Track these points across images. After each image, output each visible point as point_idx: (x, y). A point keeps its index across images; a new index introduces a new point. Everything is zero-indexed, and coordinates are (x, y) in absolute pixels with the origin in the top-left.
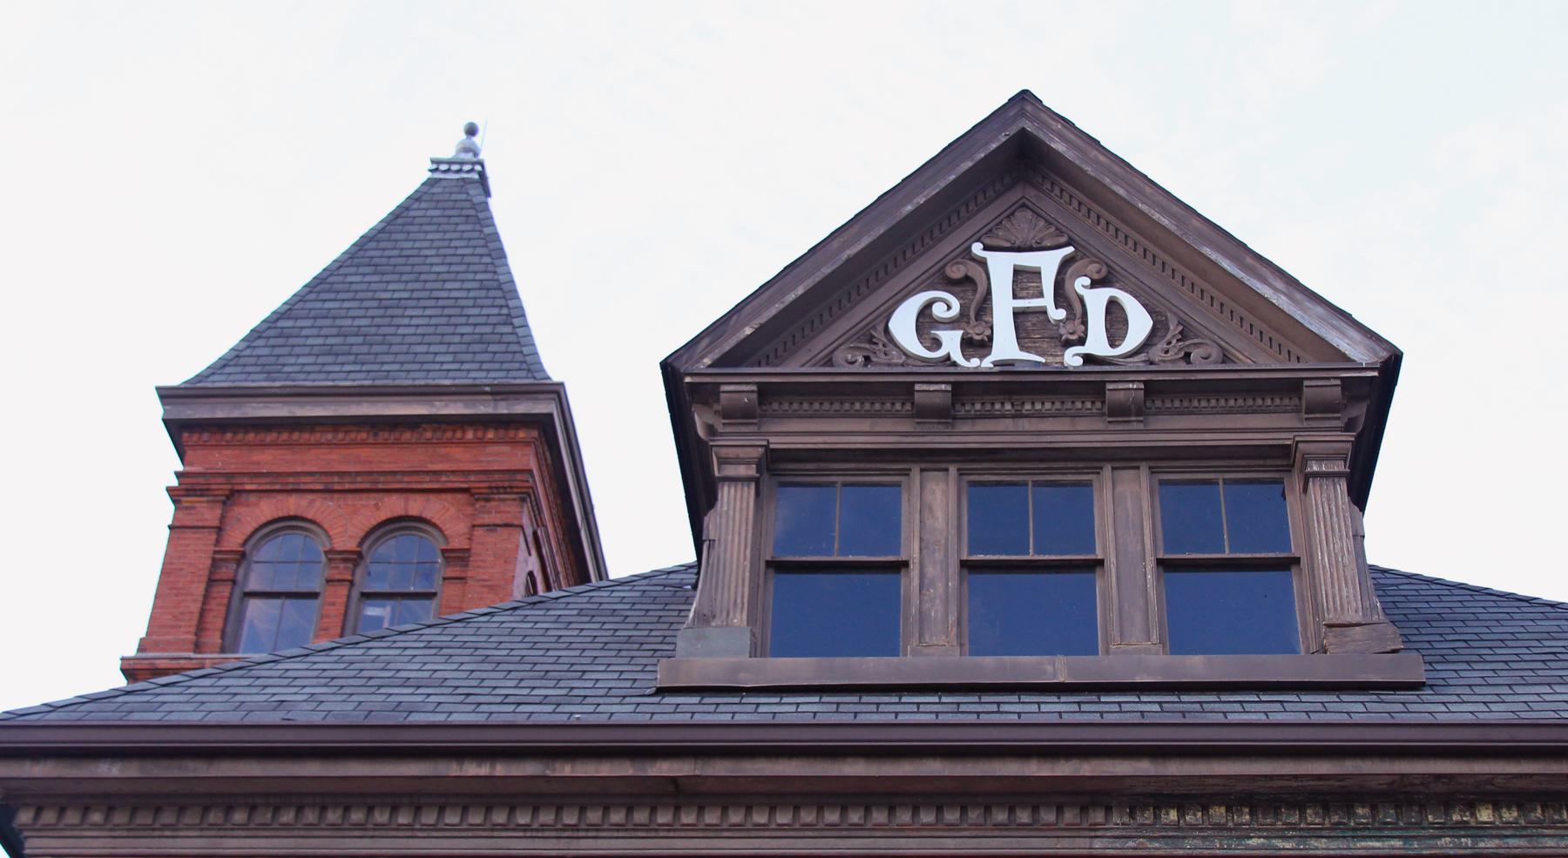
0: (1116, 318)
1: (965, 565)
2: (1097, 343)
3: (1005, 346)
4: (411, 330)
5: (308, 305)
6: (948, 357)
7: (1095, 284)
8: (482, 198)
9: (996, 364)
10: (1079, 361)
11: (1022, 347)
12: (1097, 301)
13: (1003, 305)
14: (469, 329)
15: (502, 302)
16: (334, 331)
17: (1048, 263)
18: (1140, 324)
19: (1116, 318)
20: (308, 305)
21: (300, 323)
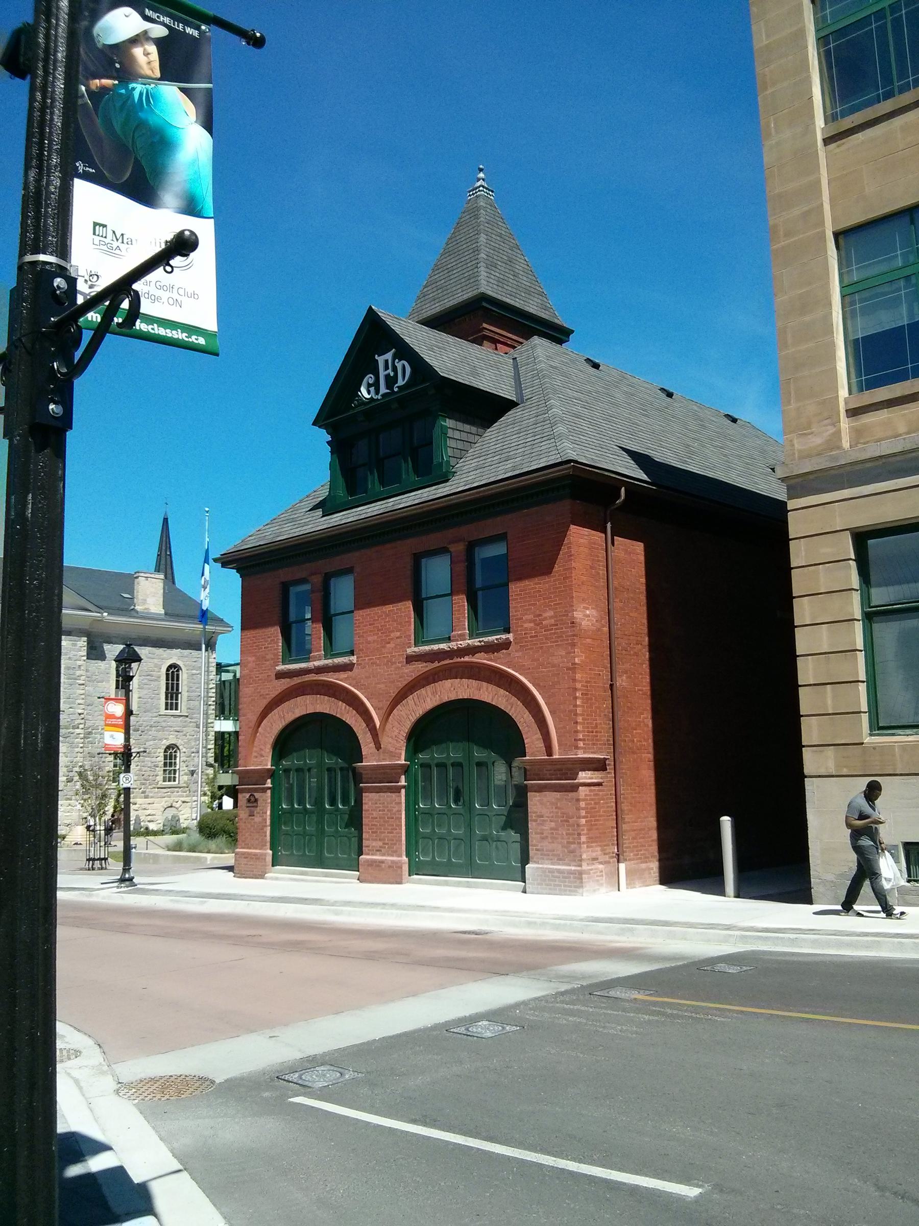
2: (401, 382)
3: (383, 390)
12: (399, 365)
13: (382, 374)
17: (389, 356)
18: (408, 370)
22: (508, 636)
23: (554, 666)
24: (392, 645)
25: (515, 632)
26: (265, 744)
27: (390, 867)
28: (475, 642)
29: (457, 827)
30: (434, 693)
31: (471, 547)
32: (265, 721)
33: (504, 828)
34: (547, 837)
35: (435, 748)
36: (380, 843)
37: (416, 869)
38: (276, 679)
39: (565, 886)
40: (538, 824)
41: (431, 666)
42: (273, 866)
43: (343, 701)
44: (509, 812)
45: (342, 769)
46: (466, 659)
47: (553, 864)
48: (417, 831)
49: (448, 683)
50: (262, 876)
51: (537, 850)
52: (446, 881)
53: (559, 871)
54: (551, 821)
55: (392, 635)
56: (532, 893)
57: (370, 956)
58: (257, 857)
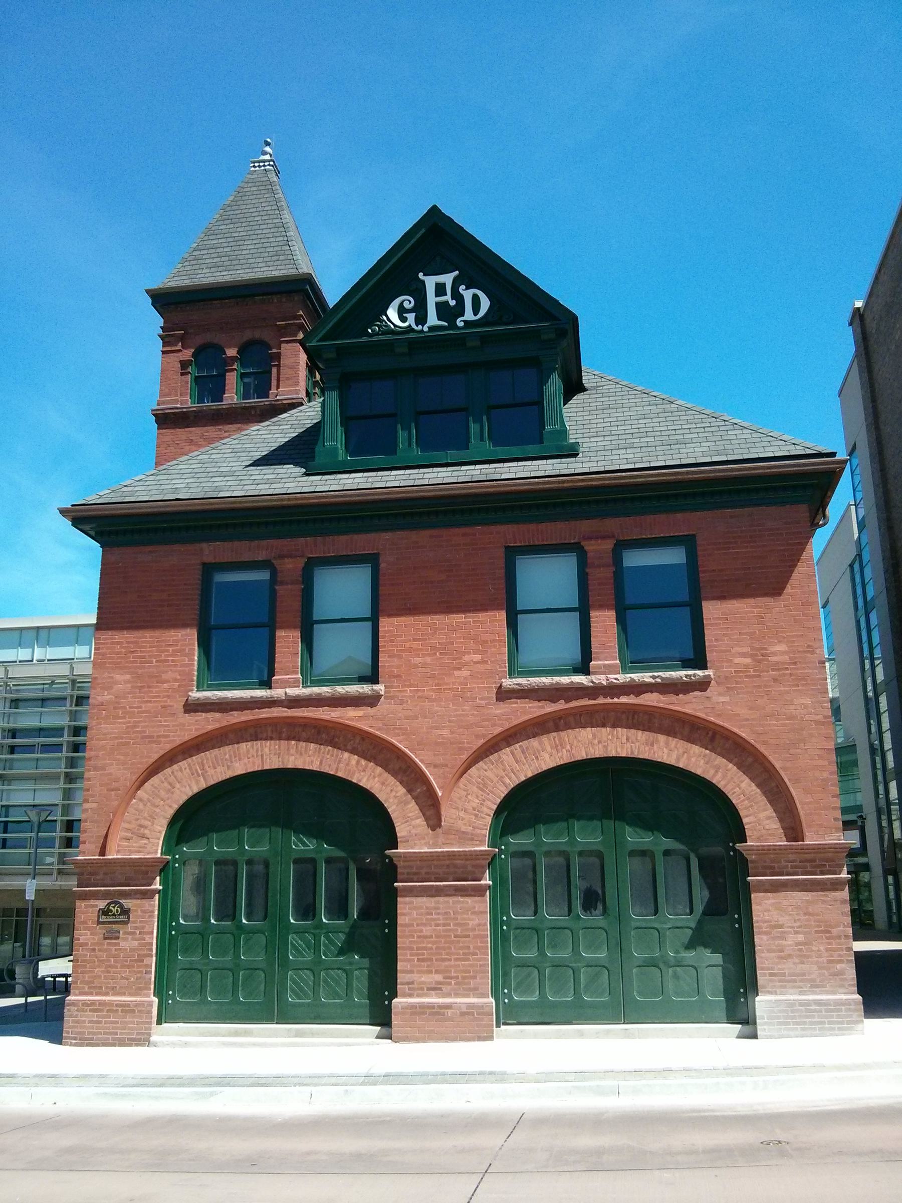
0: (476, 301)
1: (163, 352)
2: (469, 315)
3: (433, 319)
4: (247, 252)
5: (205, 243)
6: (410, 326)
7: (466, 289)
8: (349, 747)
9: (429, 328)
10: (462, 324)
11: (439, 320)
12: (468, 295)
13: (432, 300)
14: (271, 249)
15: (284, 234)
16: (216, 255)
17: (448, 279)
18: (485, 304)
19: (476, 301)
20: (205, 243)
21: (203, 252)
22: (707, 672)
23: (791, 718)
24: (465, 673)
25: (716, 669)
26: (152, 817)
27: (463, 1014)
28: (622, 678)
29: (593, 946)
30: (557, 747)
31: (209, 569)
32: (155, 780)
33: (691, 945)
34: (790, 956)
35: (542, 828)
36: (439, 977)
37: (511, 1014)
38: (186, 711)
39: (830, 1023)
40: (774, 938)
41: (550, 708)
42: (159, 1022)
43: (353, 751)
44: (700, 922)
45: (328, 861)
46: (624, 699)
47: (801, 993)
48: (507, 957)
49: (587, 734)
50: (490, 1038)
51: (771, 975)
52: (579, 1031)
53: (819, 1003)
54: (796, 933)
55: (466, 658)
56: (771, 1037)
57: (719, 1157)
58: (126, 1009)
